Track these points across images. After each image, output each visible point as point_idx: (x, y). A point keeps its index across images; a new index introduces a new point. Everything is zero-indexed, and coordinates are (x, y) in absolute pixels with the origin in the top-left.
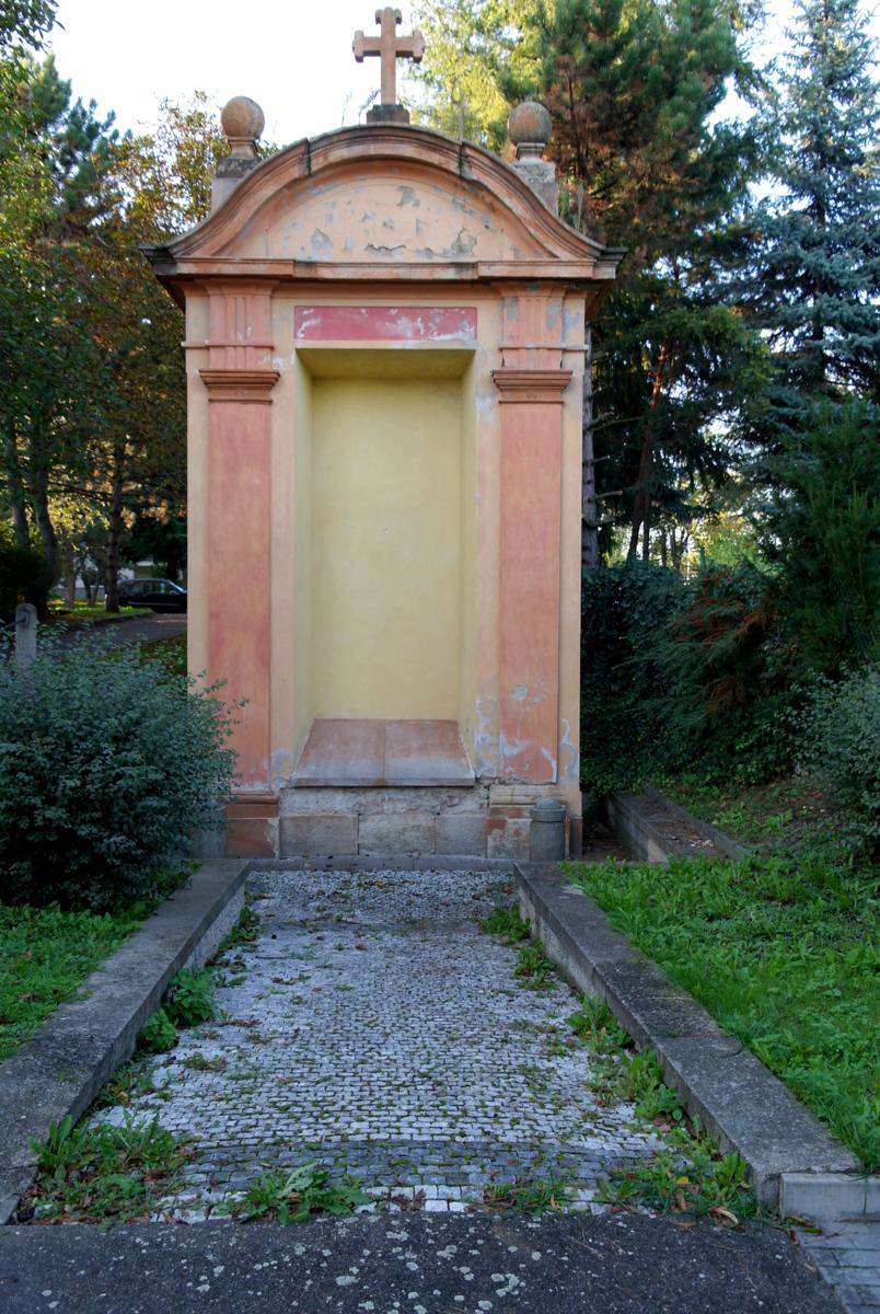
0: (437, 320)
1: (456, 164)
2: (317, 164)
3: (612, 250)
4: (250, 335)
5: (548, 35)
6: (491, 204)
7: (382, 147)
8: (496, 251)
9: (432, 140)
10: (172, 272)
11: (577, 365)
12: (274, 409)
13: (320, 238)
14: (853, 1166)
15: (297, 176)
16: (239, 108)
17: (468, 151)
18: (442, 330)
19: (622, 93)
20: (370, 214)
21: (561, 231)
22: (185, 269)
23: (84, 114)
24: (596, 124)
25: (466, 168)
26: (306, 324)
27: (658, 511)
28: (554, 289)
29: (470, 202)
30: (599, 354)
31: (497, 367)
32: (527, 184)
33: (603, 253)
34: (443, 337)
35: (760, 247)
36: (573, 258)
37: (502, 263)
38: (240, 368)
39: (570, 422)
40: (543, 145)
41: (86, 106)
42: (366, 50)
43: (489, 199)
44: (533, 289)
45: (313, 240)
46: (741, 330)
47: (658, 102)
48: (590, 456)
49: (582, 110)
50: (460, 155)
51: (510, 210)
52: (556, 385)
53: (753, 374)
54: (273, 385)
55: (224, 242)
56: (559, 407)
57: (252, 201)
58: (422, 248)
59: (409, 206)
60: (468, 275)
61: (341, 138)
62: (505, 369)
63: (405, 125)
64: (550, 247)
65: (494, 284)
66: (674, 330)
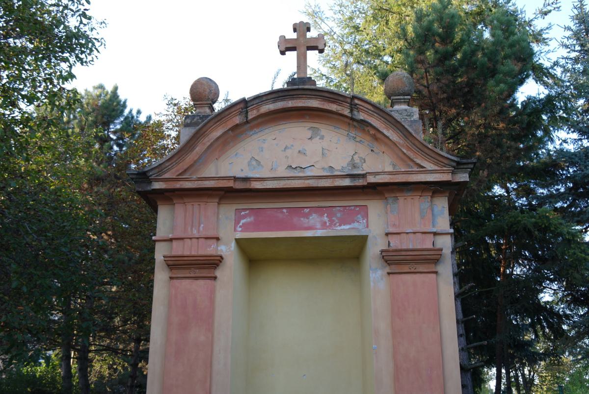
0: (339, 215)
1: (349, 111)
2: (251, 116)
3: (464, 161)
4: (202, 230)
5: (410, 45)
6: (374, 135)
7: (296, 102)
8: (379, 165)
9: (332, 96)
10: (149, 188)
11: (446, 243)
12: (218, 283)
13: (254, 163)
14: (391, 245)
15: (238, 122)
16: (202, 84)
17: (356, 101)
18: (343, 222)
19: (460, 76)
20: (289, 146)
21: (426, 150)
22: (157, 186)
23: (133, 117)
24: (445, 95)
25: (355, 113)
26: (243, 221)
27: (513, 357)
28: (423, 191)
29: (360, 135)
30: (460, 244)
31: (385, 248)
32: (399, 120)
33: (458, 163)
34: (343, 227)
35: (564, 172)
36: (436, 168)
37: (384, 173)
38: (193, 253)
39: (444, 287)
40: (409, 97)
41: (134, 113)
42: (286, 47)
43: (372, 132)
44: (410, 190)
45: (249, 164)
46: (561, 224)
47: (485, 79)
48: (461, 316)
49: (434, 88)
50: (351, 104)
51: (387, 137)
52: (432, 259)
53: (575, 254)
54: (218, 265)
55: (185, 167)
56: (434, 276)
57: (207, 139)
58: (326, 167)
59: (316, 140)
60: (360, 182)
61: (269, 97)
62: (391, 249)
63: (313, 87)
64: (418, 161)
65: (379, 188)
66: (512, 226)
